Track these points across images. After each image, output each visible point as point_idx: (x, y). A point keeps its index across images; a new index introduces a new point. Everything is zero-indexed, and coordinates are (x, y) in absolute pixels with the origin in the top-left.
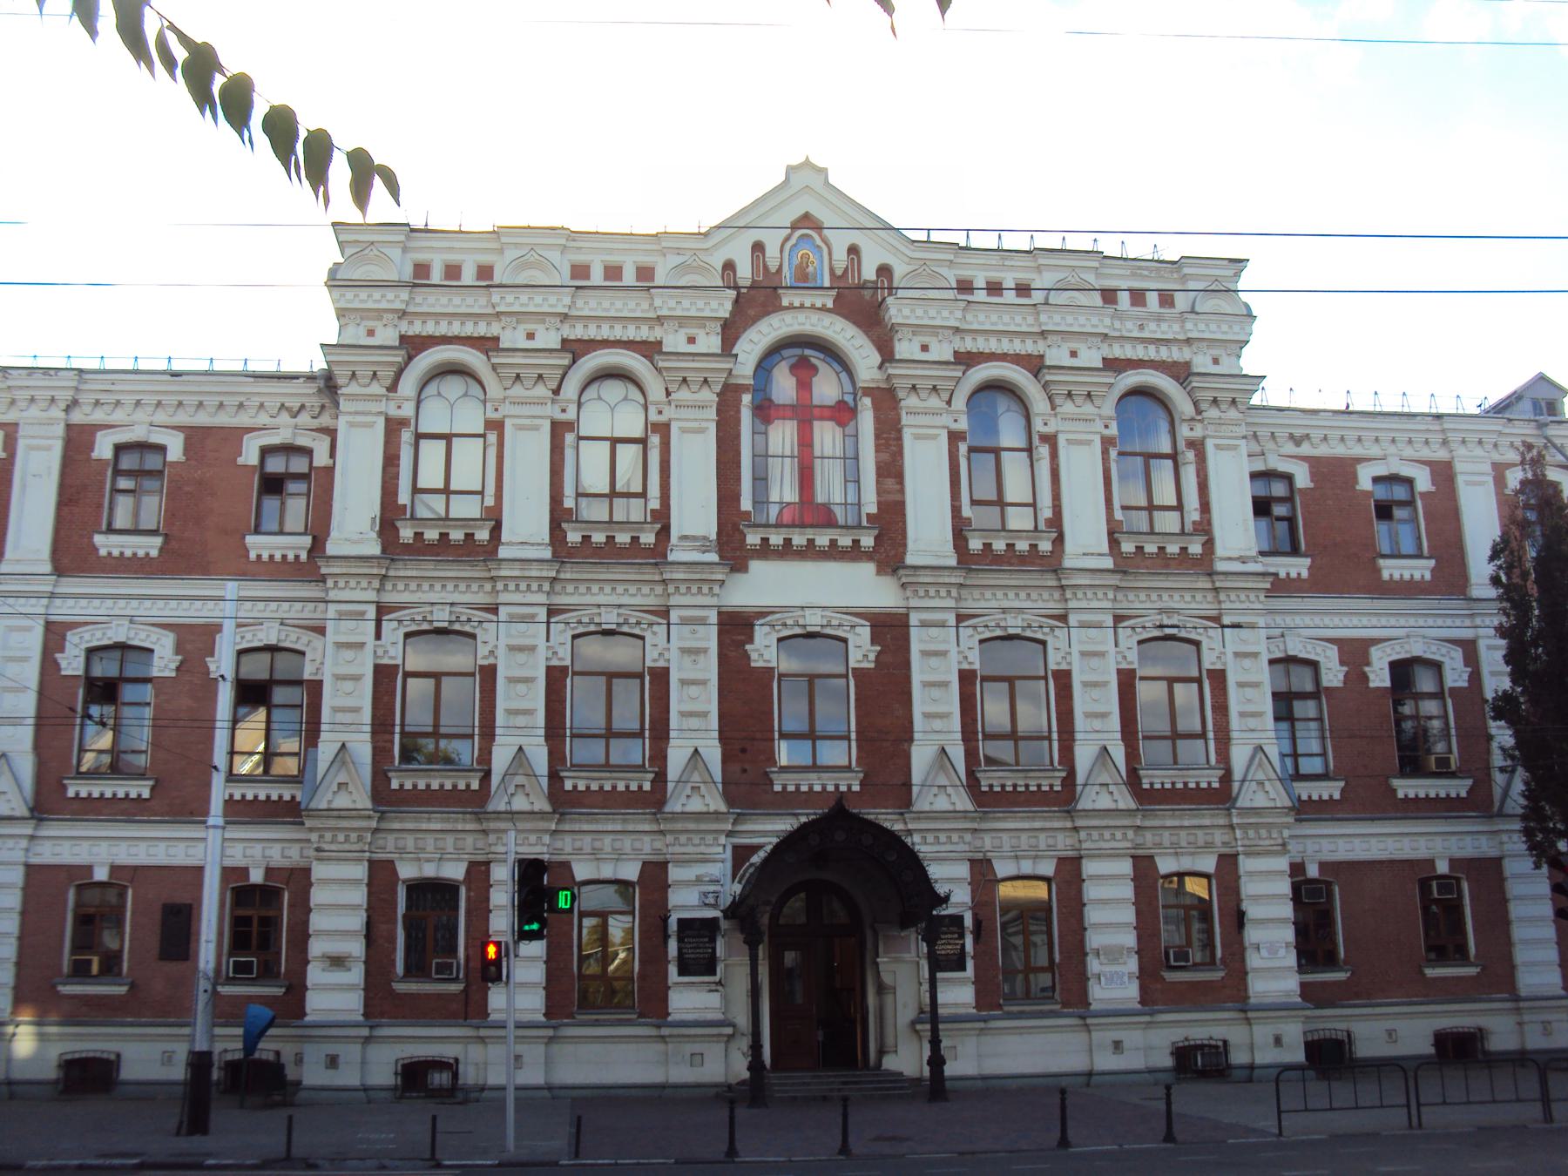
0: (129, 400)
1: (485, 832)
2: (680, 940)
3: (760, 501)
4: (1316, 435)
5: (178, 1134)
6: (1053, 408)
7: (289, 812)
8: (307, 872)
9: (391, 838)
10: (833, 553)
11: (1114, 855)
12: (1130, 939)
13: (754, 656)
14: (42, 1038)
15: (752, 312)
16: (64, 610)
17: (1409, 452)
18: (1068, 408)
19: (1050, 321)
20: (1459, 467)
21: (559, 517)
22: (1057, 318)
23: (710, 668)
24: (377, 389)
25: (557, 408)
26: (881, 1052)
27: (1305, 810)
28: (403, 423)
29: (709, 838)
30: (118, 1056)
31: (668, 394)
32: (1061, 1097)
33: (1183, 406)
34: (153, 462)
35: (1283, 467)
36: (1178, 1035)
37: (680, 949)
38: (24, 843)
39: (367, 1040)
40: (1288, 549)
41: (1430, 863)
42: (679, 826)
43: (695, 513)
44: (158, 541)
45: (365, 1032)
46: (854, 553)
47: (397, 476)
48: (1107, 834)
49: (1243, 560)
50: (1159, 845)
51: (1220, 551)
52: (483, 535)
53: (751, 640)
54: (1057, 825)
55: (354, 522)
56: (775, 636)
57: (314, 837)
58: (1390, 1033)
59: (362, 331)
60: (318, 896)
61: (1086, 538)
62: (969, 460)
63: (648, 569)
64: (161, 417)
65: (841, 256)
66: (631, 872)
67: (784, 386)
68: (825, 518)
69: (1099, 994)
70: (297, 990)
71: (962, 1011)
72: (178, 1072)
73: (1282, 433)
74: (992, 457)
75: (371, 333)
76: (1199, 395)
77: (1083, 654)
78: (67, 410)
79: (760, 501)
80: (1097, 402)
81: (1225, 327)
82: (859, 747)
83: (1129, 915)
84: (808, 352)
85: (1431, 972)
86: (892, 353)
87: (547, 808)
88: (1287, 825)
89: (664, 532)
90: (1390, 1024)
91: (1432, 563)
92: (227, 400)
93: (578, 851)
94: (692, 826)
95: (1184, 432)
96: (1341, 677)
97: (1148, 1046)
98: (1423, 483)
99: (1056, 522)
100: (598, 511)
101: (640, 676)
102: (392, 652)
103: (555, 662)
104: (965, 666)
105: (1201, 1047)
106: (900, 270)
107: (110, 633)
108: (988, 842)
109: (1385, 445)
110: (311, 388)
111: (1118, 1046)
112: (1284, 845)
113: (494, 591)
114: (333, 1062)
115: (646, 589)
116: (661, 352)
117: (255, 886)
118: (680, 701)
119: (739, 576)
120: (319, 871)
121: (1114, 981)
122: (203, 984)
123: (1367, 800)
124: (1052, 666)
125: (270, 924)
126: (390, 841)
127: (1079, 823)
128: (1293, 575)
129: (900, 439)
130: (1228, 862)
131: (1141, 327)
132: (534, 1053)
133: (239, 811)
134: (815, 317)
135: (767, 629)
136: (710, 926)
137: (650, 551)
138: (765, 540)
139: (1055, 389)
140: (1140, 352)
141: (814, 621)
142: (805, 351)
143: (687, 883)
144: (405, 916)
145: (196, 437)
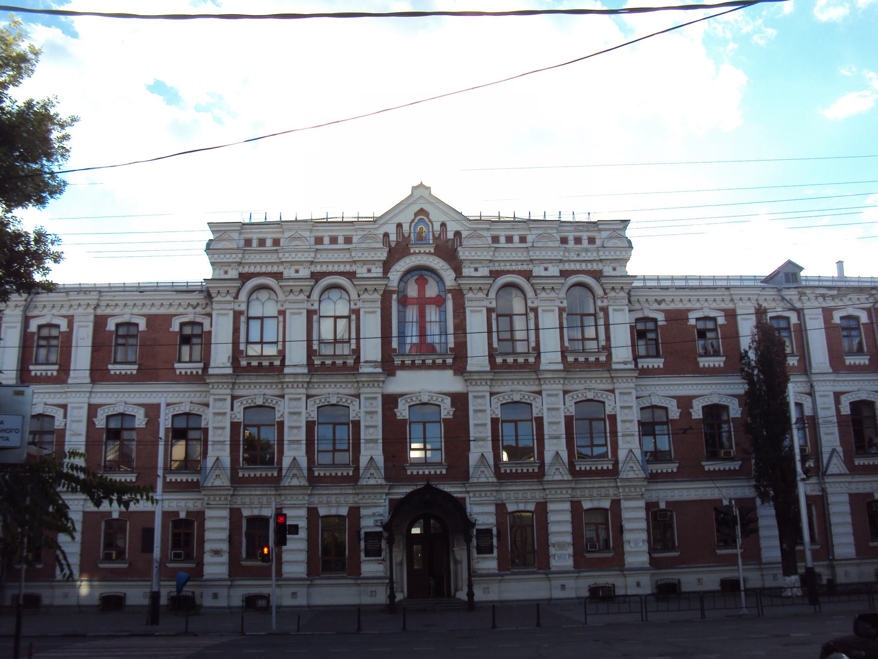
0: (121, 303)
1: (280, 495)
2: (366, 542)
3: (402, 343)
4: (668, 299)
5: (147, 625)
6: (536, 295)
7: (193, 487)
8: (203, 513)
9: (239, 498)
10: (434, 366)
11: (562, 501)
12: (569, 539)
13: (398, 414)
14: (91, 587)
15: (397, 256)
16: (96, 400)
17: (714, 305)
18: (543, 295)
19: (534, 254)
20: (739, 312)
21: (311, 353)
22: (537, 253)
23: (378, 420)
24: (229, 298)
25: (309, 304)
26: (456, 590)
27: (653, 478)
28: (241, 313)
29: (378, 496)
30: (125, 594)
31: (359, 296)
32: (537, 610)
33: (599, 292)
34: (133, 331)
35: (652, 315)
36: (591, 582)
37: (366, 546)
38: (82, 502)
39: (230, 587)
40: (655, 354)
41: (720, 501)
42: (365, 491)
43: (372, 351)
44: (136, 367)
45: (229, 583)
46: (444, 366)
47: (239, 337)
48: (559, 492)
49: (625, 363)
50: (583, 496)
51: (614, 359)
52: (277, 363)
53: (397, 407)
54: (536, 487)
55: (221, 356)
56: (407, 405)
57: (206, 498)
58: (699, 580)
59: (222, 272)
60: (208, 524)
61: (551, 358)
62: (497, 320)
63: (350, 377)
64: (136, 311)
65: (437, 227)
66: (344, 511)
67: (412, 291)
68: (431, 349)
69: (555, 564)
70: (200, 564)
71: (492, 571)
72: (146, 602)
73: (651, 299)
74: (508, 319)
75: (226, 272)
76: (605, 286)
77: (549, 409)
78: (95, 309)
79: (402, 343)
80: (557, 292)
81: (618, 253)
82: (446, 454)
83: (569, 528)
84: (423, 272)
85: (719, 552)
86: (461, 273)
87: (307, 484)
88: (644, 486)
89: (357, 360)
90: (700, 576)
91: (724, 358)
92: (164, 302)
93: (321, 503)
94: (370, 491)
95: (599, 303)
96: (678, 414)
97: (577, 587)
98: (721, 321)
99: (537, 348)
100: (328, 350)
101: (348, 424)
102: (238, 416)
103: (310, 419)
104: (494, 416)
105: (602, 587)
106: (464, 234)
107: (116, 409)
108: (504, 495)
109: (702, 302)
110: (202, 296)
111: (563, 587)
112: (642, 495)
113: (282, 388)
114: (215, 596)
115: (350, 385)
116: (355, 278)
117: (182, 520)
118: (365, 435)
119: (391, 378)
120: (209, 513)
121: (562, 557)
122: (156, 564)
123: (690, 472)
124: (534, 415)
125: (189, 536)
126: (239, 500)
127: (545, 487)
128: (656, 366)
129: (465, 312)
130: (616, 503)
131: (578, 255)
132: (302, 591)
133: (169, 487)
134: (425, 257)
135: (404, 401)
136: (378, 535)
137: (350, 367)
138: (403, 362)
139: (536, 287)
140: (578, 267)
141: (425, 399)
142: (421, 273)
143: (369, 516)
144: (246, 533)
145: (151, 319)
